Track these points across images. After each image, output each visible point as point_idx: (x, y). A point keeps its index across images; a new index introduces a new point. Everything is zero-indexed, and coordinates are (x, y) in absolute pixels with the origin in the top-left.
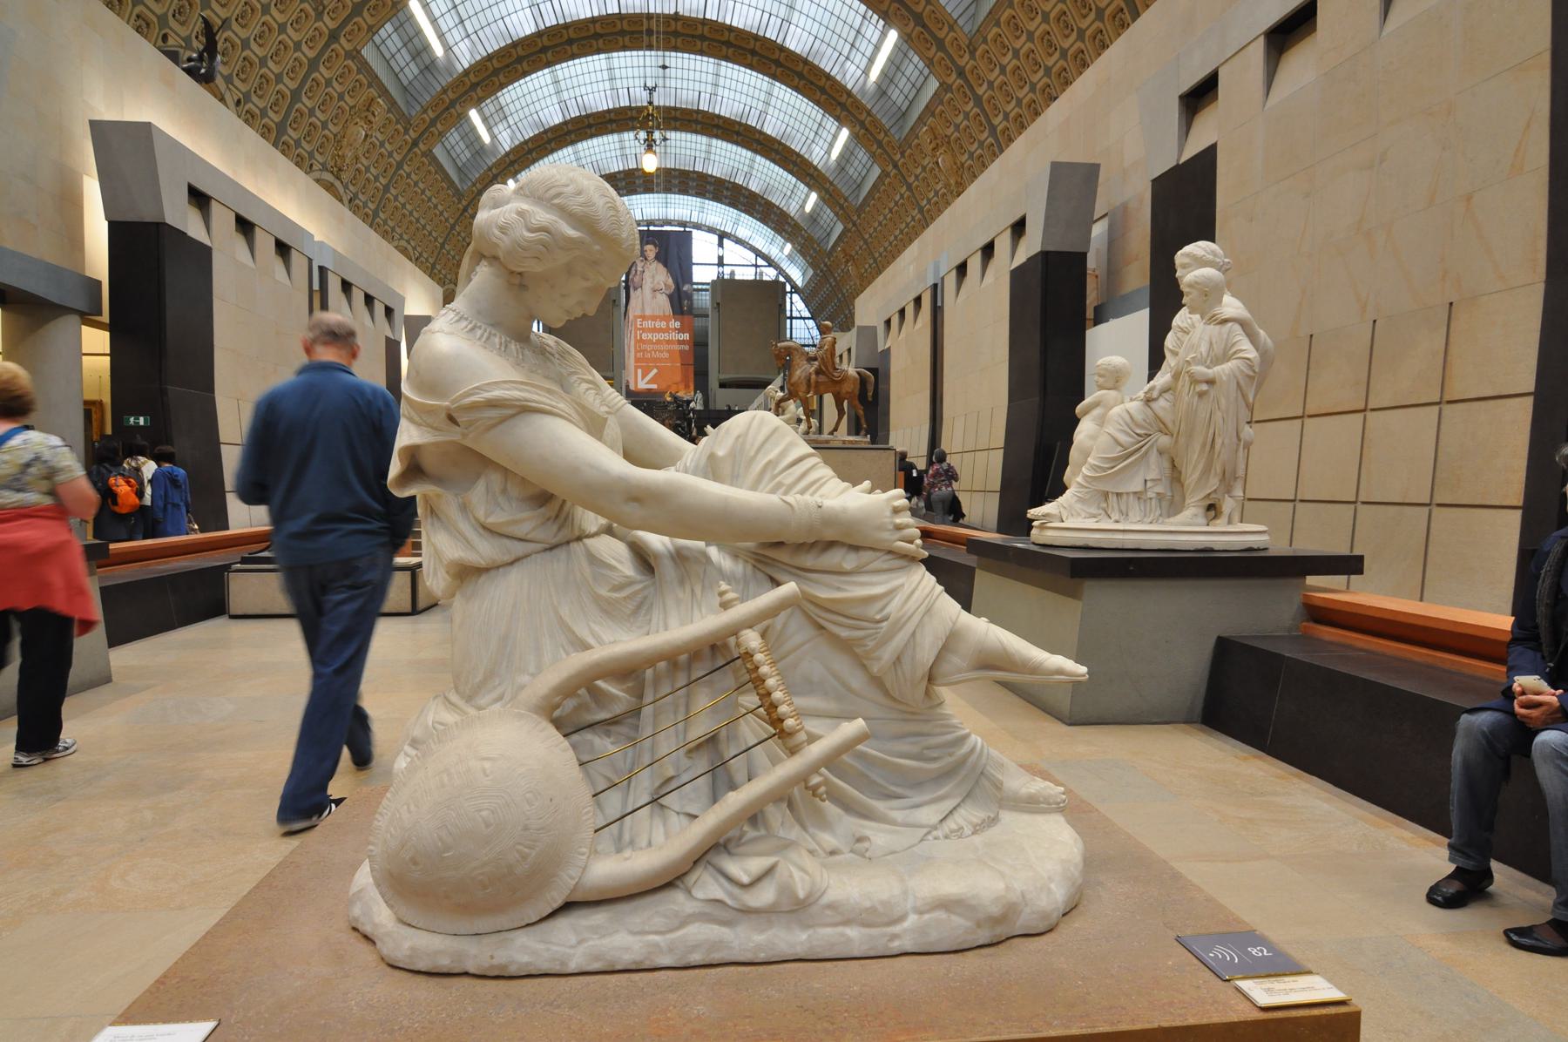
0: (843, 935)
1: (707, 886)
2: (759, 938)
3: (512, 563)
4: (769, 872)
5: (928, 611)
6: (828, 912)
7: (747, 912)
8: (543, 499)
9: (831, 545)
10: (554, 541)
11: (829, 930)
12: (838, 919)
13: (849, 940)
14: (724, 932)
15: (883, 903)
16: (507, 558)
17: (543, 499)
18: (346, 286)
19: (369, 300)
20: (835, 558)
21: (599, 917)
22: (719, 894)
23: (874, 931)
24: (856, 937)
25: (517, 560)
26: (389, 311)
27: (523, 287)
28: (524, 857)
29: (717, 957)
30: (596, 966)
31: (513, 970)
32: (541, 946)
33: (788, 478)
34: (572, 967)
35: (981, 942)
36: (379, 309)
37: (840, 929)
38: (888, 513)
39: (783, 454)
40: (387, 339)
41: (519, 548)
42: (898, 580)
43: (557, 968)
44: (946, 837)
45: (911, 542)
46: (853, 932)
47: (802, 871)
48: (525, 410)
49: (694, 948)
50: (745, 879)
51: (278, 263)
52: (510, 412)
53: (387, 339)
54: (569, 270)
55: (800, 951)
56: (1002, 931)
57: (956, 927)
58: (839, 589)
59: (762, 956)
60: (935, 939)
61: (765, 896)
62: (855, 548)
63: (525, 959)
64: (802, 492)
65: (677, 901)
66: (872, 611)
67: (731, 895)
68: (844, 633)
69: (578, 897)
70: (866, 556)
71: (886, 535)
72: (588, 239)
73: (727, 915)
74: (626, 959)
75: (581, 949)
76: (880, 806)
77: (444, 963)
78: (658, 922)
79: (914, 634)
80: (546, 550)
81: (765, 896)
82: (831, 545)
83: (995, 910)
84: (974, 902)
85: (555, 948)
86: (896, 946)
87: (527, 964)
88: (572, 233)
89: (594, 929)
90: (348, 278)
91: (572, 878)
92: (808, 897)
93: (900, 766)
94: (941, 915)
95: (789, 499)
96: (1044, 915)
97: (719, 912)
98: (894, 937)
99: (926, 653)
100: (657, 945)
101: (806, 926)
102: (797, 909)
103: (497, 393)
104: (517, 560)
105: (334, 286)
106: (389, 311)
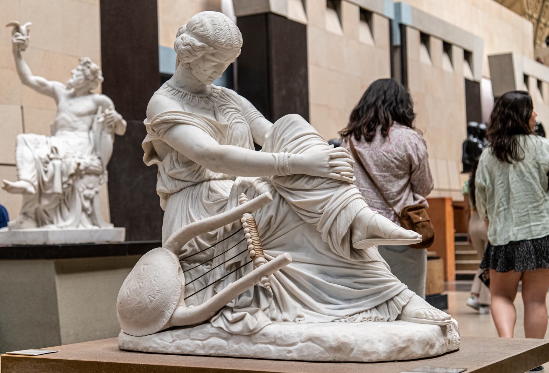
0: (268, 348)
1: (220, 322)
2: (236, 346)
3: (179, 191)
4: (242, 318)
5: (344, 208)
6: (263, 337)
7: (232, 334)
8: (188, 163)
9: (302, 176)
10: (197, 181)
11: (263, 346)
12: (267, 341)
13: (270, 351)
14: (223, 342)
15: (285, 336)
16: (175, 190)
17: (188, 163)
18: (425, 38)
19: (447, 47)
20: (301, 184)
21: (180, 332)
22: (223, 326)
23: (280, 348)
24: (273, 350)
25: (181, 190)
26: (468, 55)
27: (191, 69)
28: (151, 301)
29: (220, 352)
30: (178, 351)
31: (151, 350)
32: (159, 341)
33: (289, 147)
34: (170, 350)
35: (328, 360)
36: (458, 53)
37: (269, 346)
38: (327, 158)
39: (291, 135)
40: (468, 82)
41: (182, 185)
42: (329, 193)
43: (165, 351)
44: (346, 321)
45: (339, 173)
46: (272, 348)
47: (258, 320)
48: (176, 124)
49: (212, 347)
50: (230, 319)
51: (363, 29)
52: (170, 125)
53: (468, 82)
54: (203, 58)
55: (251, 354)
56: (338, 356)
57: (316, 351)
58: (304, 198)
59: (237, 354)
60: (306, 354)
61: (237, 328)
62: (313, 178)
63: (155, 346)
64: (296, 153)
65: (208, 328)
66: (317, 209)
67: (226, 326)
68: (309, 221)
69: (175, 323)
70: (315, 182)
71: (325, 170)
72: (206, 46)
73: (225, 335)
74: (188, 349)
75: (174, 344)
76: (322, 307)
77: (131, 346)
78: (200, 336)
79: (336, 218)
80: (193, 185)
81: (237, 328)
82: (302, 176)
83: (334, 344)
84: (325, 339)
85: (164, 342)
86: (290, 356)
87: (156, 348)
88: (198, 43)
89: (178, 336)
90: (426, 30)
91: (170, 313)
92: (255, 329)
93: (332, 286)
94: (310, 343)
95: (276, 155)
96: (366, 353)
97: (221, 333)
98: (290, 352)
99: (342, 228)
100: (199, 345)
101: (255, 343)
102: (251, 334)
103: (166, 117)
104: (181, 190)
105: (413, 37)
106: (468, 55)
